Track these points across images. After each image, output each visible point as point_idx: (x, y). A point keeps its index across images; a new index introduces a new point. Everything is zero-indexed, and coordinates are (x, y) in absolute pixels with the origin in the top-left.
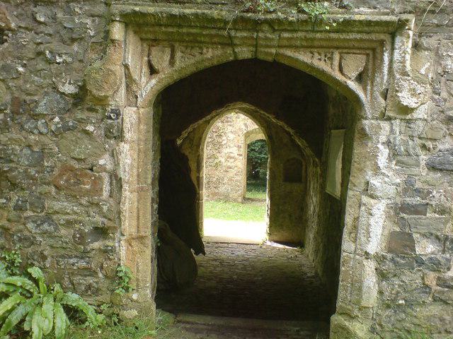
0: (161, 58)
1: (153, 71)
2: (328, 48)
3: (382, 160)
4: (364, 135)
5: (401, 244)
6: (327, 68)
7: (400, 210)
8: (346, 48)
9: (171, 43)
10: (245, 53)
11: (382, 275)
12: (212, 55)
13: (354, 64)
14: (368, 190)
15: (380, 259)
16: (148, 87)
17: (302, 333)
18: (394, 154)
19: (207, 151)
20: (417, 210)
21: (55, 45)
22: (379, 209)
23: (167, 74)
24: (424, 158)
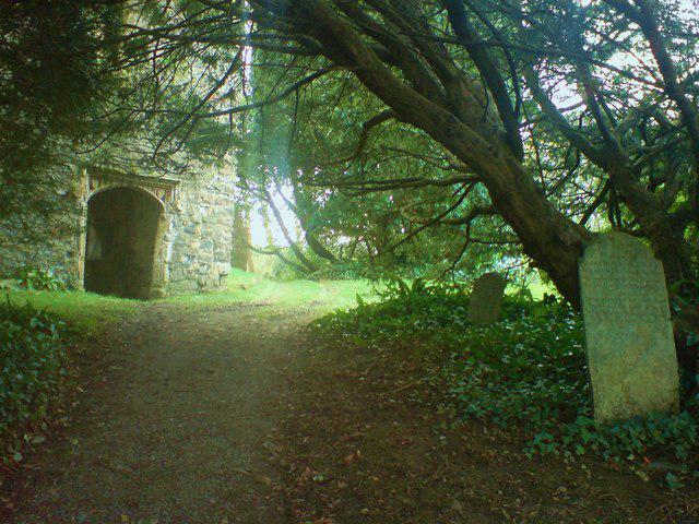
0: (95, 184)
1: (91, 188)
2: (153, 187)
3: (171, 228)
4: (163, 219)
5: (176, 257)
6: (152, 193)
7: (176, 246)
8: (161, 188)
9: (99, 179)
10: (125, 185)
11: (170, 270)
12: (115, 184)
13: (162, 193)
14: (165, 238)
15: (170, 263)
16: (90, 194)
17: (524, 22)
18: (175, 225)
19: (676, 378)
20: (181, 245)
21: (536, 418)
22: (170, 245)
23: (97, 189)
24: (183, 228)
